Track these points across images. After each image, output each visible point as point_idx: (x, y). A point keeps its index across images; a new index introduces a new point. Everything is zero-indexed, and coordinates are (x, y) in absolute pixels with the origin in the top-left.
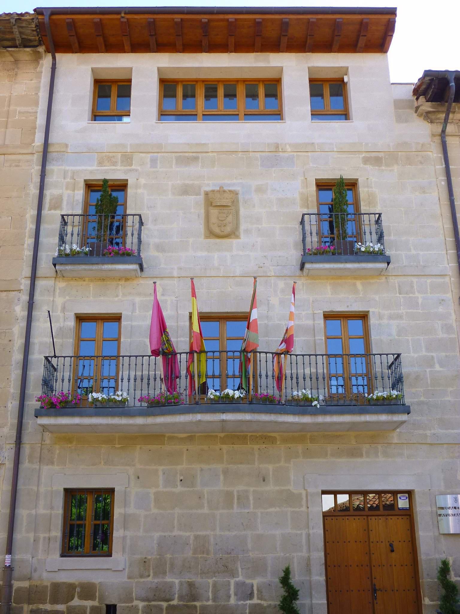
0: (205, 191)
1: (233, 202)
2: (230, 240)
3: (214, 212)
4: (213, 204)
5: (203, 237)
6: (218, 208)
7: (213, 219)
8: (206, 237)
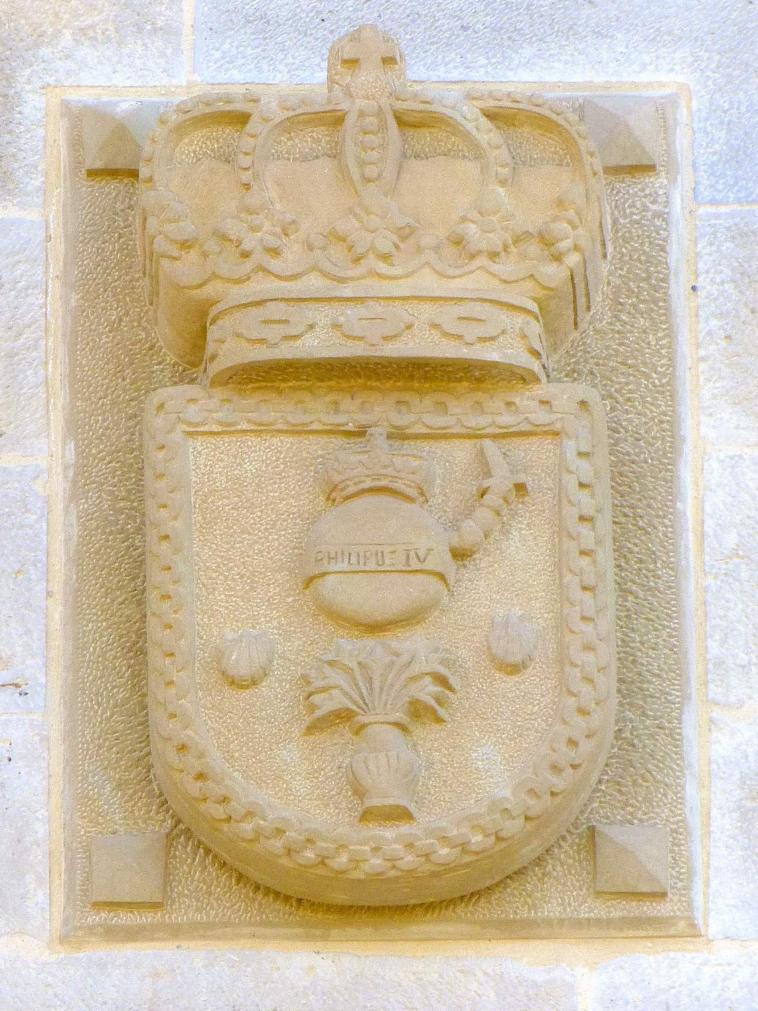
0: (80, 120)
1: (562, 309)
2: (521, 963)
3: (236, 475)
4: (230, 347)
5: (43, 898)
6: (318, 409)
7: (230, 602)
8: (107, 912)
